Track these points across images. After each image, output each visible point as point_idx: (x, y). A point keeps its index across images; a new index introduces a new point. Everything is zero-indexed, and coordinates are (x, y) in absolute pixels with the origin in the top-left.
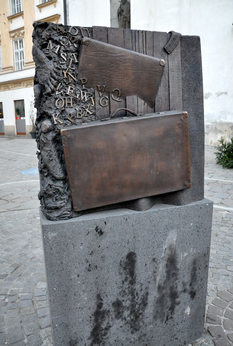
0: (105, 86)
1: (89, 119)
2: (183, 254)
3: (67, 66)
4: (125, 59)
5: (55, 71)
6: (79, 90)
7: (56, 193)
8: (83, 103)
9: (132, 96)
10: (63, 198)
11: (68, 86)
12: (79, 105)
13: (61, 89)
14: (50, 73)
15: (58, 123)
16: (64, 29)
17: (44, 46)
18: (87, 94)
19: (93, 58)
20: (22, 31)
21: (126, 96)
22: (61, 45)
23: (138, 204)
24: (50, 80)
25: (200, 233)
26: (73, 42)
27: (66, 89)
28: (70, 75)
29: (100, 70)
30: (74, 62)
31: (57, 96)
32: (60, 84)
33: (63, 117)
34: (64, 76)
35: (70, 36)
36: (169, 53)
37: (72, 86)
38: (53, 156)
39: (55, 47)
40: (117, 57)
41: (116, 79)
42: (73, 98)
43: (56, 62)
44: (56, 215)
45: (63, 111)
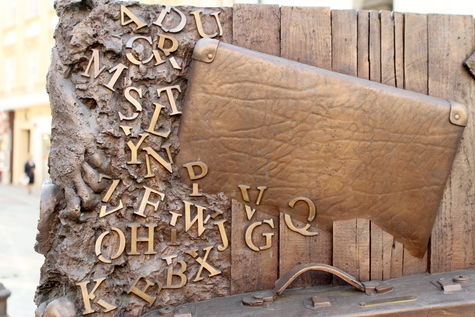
1: (208, 291)
3: (144, 127)
4: (331, 106)
8: (190, 238)
9: (354, 220)
13: (120, 197)
14: (82, 150)
17: (76, 67)
22: (129, 64)
24: (83, 173)
28: (150, 155)
31: (103, 221)
32: (116, 182)
34: (130, 158)
37: (156, 187)
40: (303, 98)
41: (301, 168)
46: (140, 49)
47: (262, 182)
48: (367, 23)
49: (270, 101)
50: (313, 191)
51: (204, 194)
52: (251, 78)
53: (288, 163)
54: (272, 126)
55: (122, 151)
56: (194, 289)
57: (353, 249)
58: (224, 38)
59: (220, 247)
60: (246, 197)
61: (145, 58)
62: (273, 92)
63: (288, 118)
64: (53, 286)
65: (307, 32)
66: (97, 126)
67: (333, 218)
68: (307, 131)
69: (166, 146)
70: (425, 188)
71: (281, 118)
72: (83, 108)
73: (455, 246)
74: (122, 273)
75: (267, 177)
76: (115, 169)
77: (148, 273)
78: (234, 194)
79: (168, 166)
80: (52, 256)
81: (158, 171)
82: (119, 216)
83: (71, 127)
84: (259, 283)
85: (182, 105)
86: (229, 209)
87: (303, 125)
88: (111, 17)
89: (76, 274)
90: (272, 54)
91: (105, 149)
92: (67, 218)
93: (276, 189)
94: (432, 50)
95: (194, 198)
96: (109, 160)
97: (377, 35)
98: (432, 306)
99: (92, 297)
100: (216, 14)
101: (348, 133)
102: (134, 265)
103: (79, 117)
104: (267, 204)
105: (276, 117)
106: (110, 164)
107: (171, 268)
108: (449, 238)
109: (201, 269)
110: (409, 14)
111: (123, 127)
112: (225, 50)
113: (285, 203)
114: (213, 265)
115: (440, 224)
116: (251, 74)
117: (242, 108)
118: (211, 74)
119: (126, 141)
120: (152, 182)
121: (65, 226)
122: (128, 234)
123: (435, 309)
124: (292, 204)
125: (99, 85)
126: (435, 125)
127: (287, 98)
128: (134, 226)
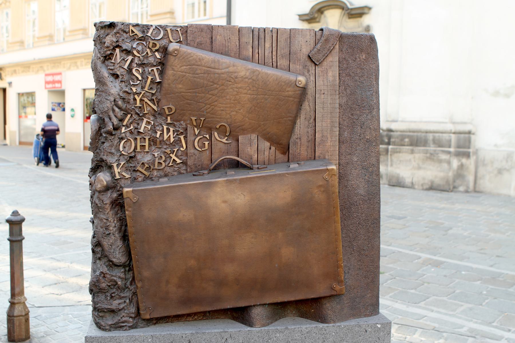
3: (143, 88)
4: (236, 78)
7: (112, 287)
9: (250, 135)
13: (131, 123)
14: (113, 99)
15: (122, 177)
17: (107, 58)
22: (135, 56)
23: (250, 315)
24: (113, 111)
32: (129, 116)
34: (136, 104)
36: (318, 63)
40: (223, 74)
41: (222, 109)
44: (110, 323)
46: (140, 48)
47: (203, 116)
48: (258, 34)
49: (206, 75)
50: (228, 120)
52: (196, 64)
53: (215, 106)
54: (207, 88)
55: (132, 100)
56: (168, 170)
57: (249, 150)
58: (183, 42)
59: (182, 149)
60: (195, 124)
61: (143, 53)
62: (207, 71)
63: (215, 84)
64: (98, 168)
65: (226, 39)
66: (119, 88)
68: (225, 90)
69: (154, 98)
70: (285, 119)
71: (212, 84)
72: (112, 79)
73: (302, 148)
74: (133, 161)
75: (205, 113)
77: (146, 161)
78: (188, 122)
79: (155, 108)
80: (98, 153)
82: (131, 132)
83: (106, 88)
84: (202, 167)
85: (162, 77)
86: (186, 130)
87: (222, 87)
88: (125, 32)
89: (111, 160)
90: (208, 50)
91: (124, 99)
92: (105, 133)
93: (210, 119)
94: (292, 48)
95: (168, 124)
97: (263, 40)
98: (281, 173)
99: (119, 171)
100: (179, 29)
101: (245, 91)
102: (139, 157)
103: (110, 83)
104: (205, 127)
105: (209, 83)
106: (126, 106)
107: (157, 159)
108: (299, 145)
110: (280, 29)
111: (133, 88)
112: (183, 49)
113: (214, 127)
114: (178, 158)
116: (196, 62)
117: (192, 78)
118: (176, 61)
119: (134, 95)
120: (147, 116)
121: (105, 137)
123: (282, 174)
124: (218, 127)
125: (120, 67)
126: (289, 87)
127: (214, 74)
128: (138, 138)
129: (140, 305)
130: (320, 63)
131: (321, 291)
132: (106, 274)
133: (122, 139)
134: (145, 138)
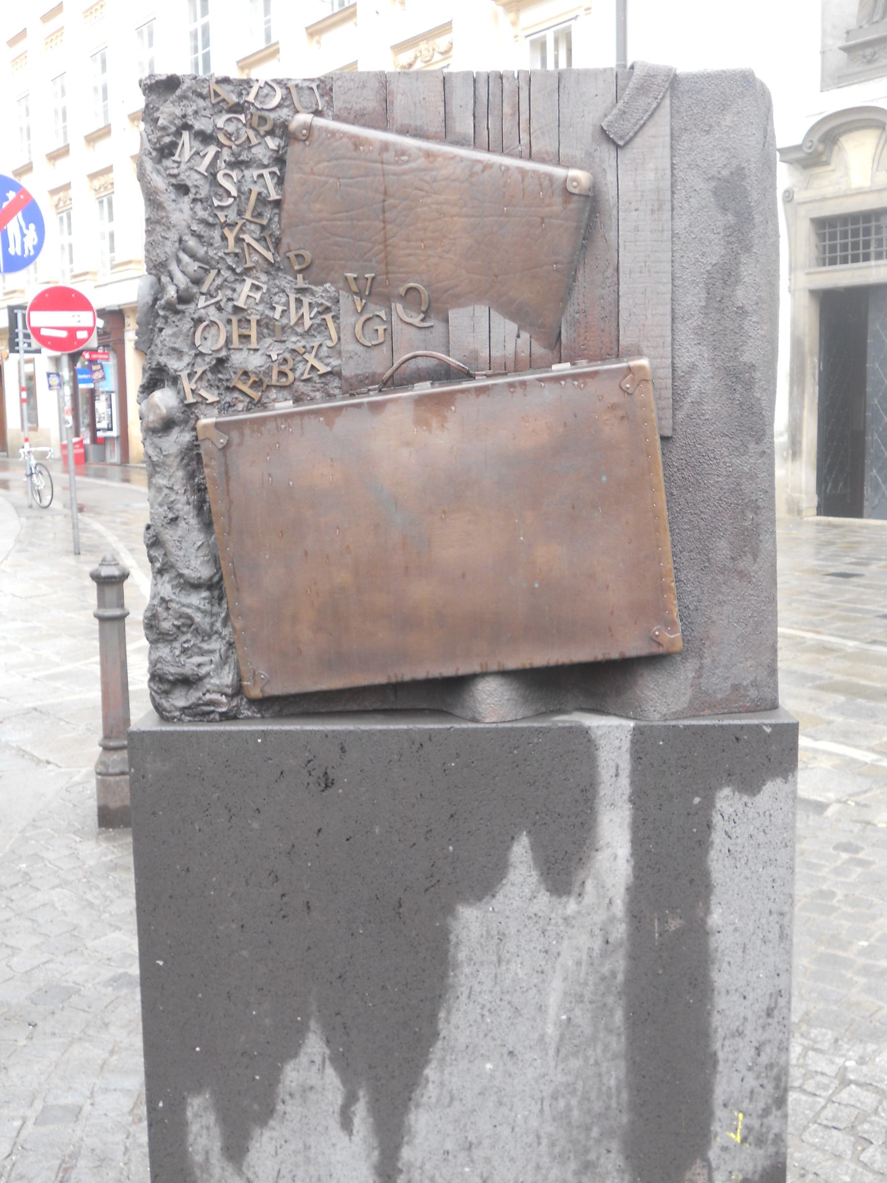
0: (373, 275)
1: (318, 390)
2: (663, 921)
3: (240, 213)
4: (435, 180)
5: (195, 231)
6: (284, 291)
7: (185, 629)
8: (297, 334)
9: (470, 308)
10: (205, 646)
11: (244, 280)
12: (284, 341)
13: (219, 288)
14: (176, 238)
15: (200, 400)
16: (236, 91)
17: (165, 151)
18: (310, 304)
19: (326, 183)
20: (442, 43)
21: (447, 310)
22: (221, 145)
23: (473, 696)
24: (179, 261)
25: (736, 844)
26: (262, 133)
27: (234, 290)
28: (248, 244)
29: (349, 222)
30: (264, 199)
31: (202, 311)
32: (214, 272)
33: (220, 380)
34: (227, 247)
35: (252, 114)
36: (621, 143)
37: (257, 278)
38: (179, 506)
39: (197, 153)
40: (405, 173)
41: (408, 251)
42: (258, 317)
43: (199, 203)
44: (181, 703)
45: (221, 363)
46: (231, 128)
51: (310, 286)
67: (448, 306)
69: (266, 234)
76: (212, 258)
79: (269, 256)
81: (257, 262)
85: (282, 190)
89: (174, 364)
92: (164, 308)
96: (205, 249)
103: (170, 203)
109: (309, 365)
114: (321, 360)
115: (571, 310)
119: (222, 228)
122: (229, 327)
129: (242, 668)
130: (627, 143)
131: (632, 646)
132: (171, 601)
133: (200, 321)
134: (249, 321)
